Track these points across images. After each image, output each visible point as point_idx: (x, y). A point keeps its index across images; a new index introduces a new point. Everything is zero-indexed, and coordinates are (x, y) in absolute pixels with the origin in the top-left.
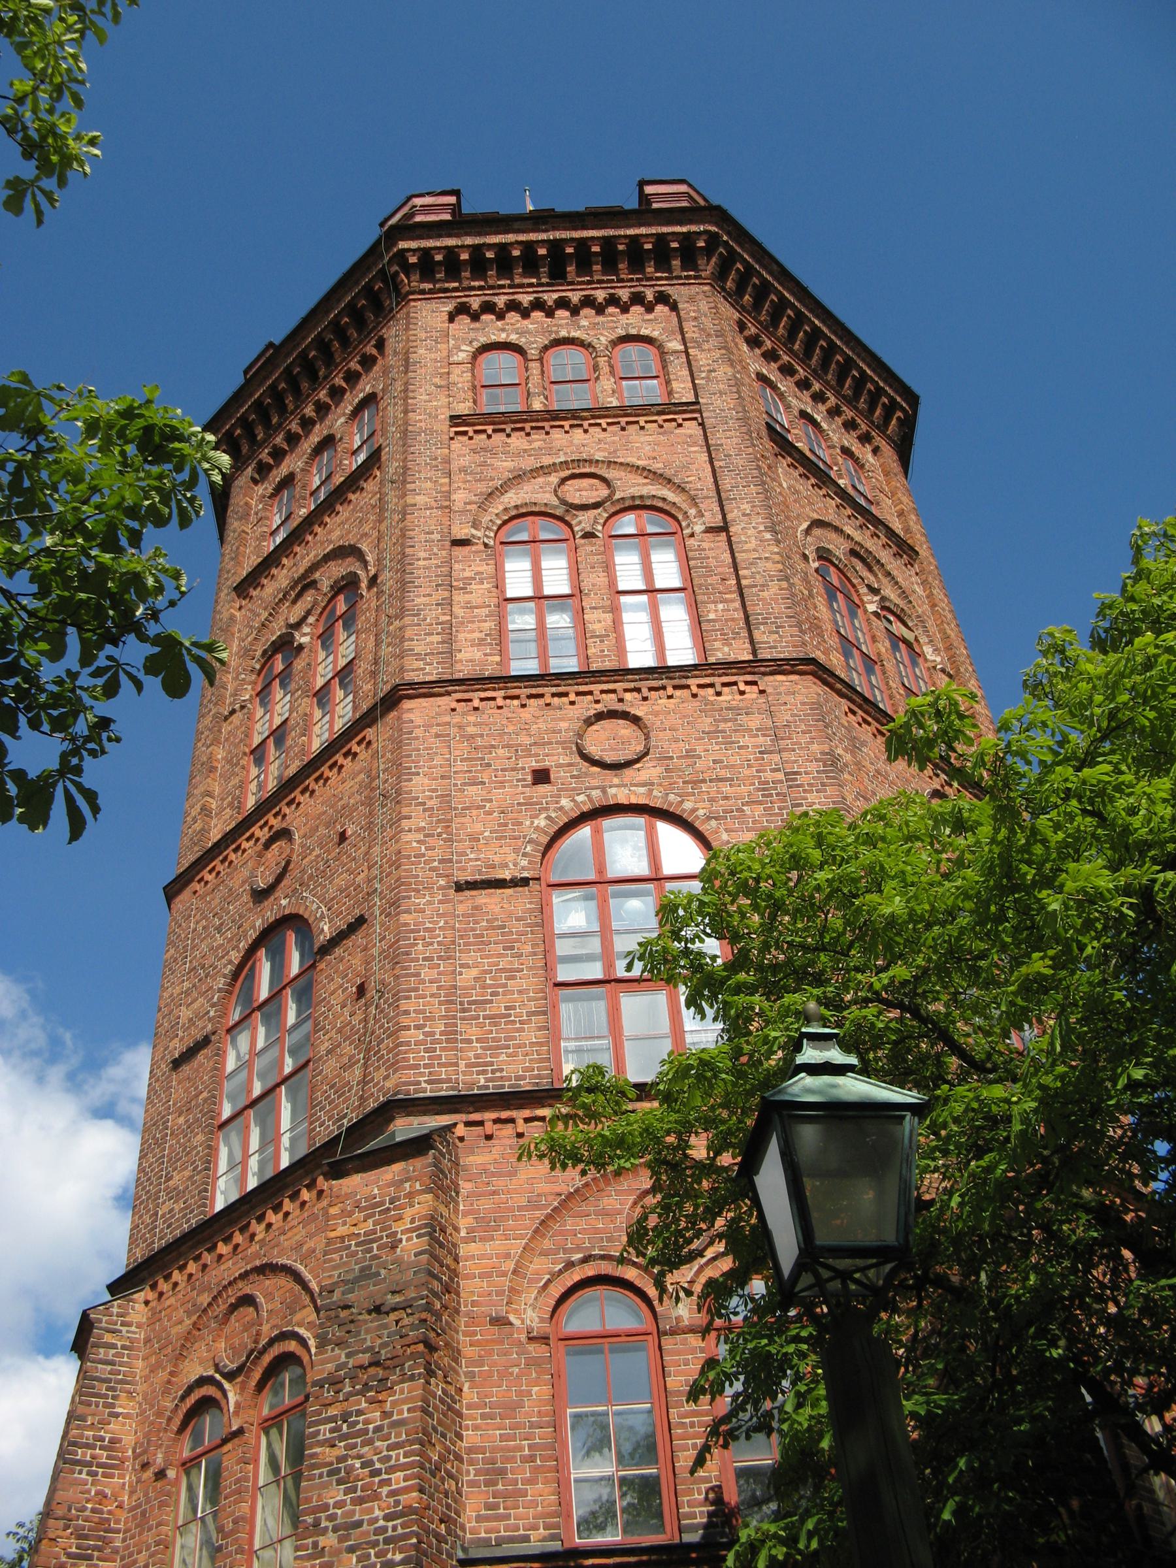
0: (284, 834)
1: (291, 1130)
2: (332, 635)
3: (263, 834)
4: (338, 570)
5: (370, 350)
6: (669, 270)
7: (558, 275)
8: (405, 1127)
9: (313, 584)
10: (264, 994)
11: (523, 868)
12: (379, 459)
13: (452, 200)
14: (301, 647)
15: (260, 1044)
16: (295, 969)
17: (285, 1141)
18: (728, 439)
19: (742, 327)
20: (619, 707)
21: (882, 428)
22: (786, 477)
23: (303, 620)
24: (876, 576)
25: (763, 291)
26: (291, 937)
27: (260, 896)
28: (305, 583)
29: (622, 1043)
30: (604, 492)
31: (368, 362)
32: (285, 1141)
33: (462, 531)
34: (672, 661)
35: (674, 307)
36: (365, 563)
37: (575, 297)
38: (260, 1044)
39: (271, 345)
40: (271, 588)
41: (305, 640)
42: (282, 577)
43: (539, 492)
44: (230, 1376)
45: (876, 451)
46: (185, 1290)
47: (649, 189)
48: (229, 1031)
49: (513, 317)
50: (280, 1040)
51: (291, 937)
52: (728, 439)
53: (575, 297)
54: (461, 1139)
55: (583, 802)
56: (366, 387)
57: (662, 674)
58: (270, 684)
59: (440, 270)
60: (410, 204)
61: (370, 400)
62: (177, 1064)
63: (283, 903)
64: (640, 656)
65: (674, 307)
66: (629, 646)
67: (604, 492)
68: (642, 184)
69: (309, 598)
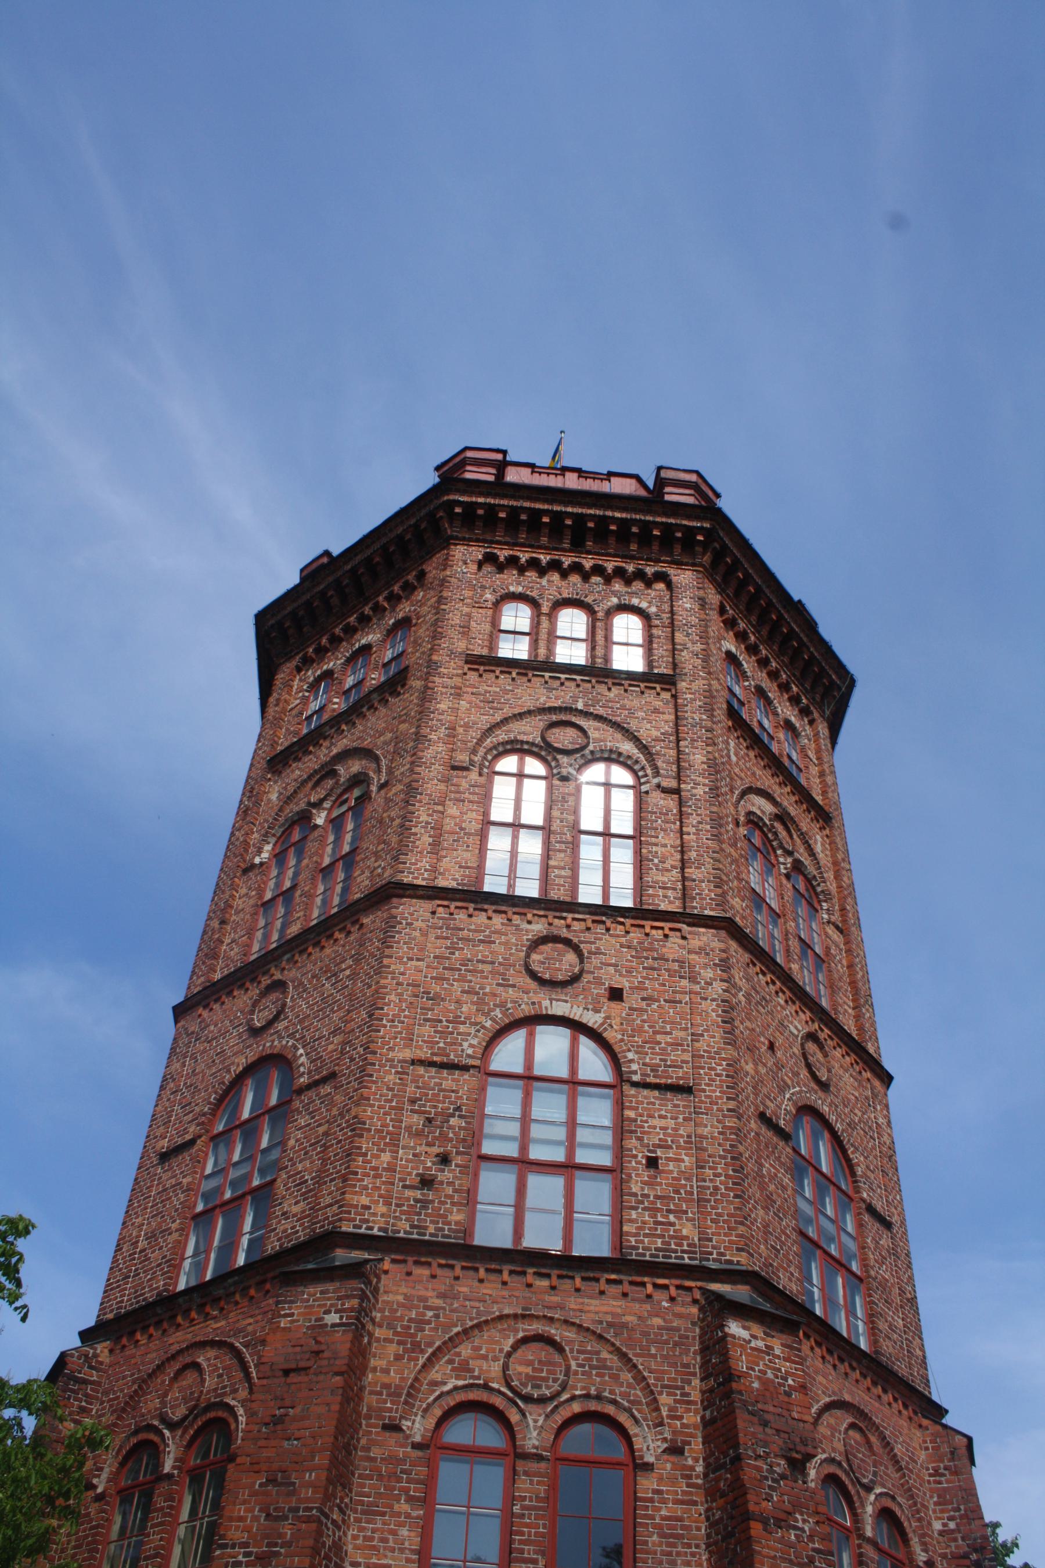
0: (280, 985)
1: (251, 1233)
2: (333, 871)
3: (265, 981)
4: (356, 766)
5: (411, 577)
6: (671, 554)
7: (577, 546)
8: (342, 1256)
9: (333, 773)
10: (246, 1115)
11: (469, 1056)
12: (405, 678)
13: (500, 457)
14: (316, 826)
15: (236, 1157)
16: (273, 1101)
17: (245, 1241)
18: (694, 714)
19: (722, 611)
20: (564, 933)
21: (820, 708)
22: (733, 748)
23: (322, 801)
24: (791, 836)
25: (742, 584)
26: (275, 1076)
27: (255, 1032)
28: (328, 771)
29: (478, 1447)
30: (581, 741)
31: (409, 589)
32: (245, 1241)
33: (463, 758)
34: (614, 902)
35: (669, 585)
36: (379, 771)
37: (588, 564)
38: (236, 1157)
39: (327, 553)
40: (298, 771)
41: (320, 821)
42: (311, 763)
43: (529, 730)
44: (172, 1426)
45: (811, 722)
46: (149, 1350)
47: (664, 474)
48: (213, 1138)
49: (532, 575)
50: (251, 1158)
51: (275, 1076)
52: (694, 714)
53: (588, 564)
54: (386, 1272)
55: (526, 1010)
56: (405, 609)
57: (604, 912)
58: (286, 850)
59: (479, 523)
60: (462, 456)
61: (405, 623)
62: (165, 1157)
63: (270, 1043)
64: (589, 894)
65: (669, 585)
66: (582, 879)
67: (581, 741)
68: (659, 469)
69: (330, 783)
